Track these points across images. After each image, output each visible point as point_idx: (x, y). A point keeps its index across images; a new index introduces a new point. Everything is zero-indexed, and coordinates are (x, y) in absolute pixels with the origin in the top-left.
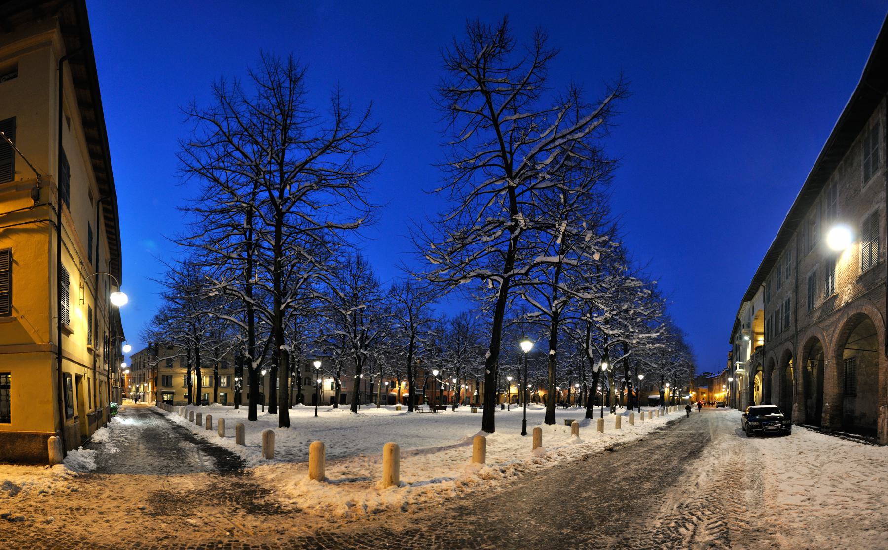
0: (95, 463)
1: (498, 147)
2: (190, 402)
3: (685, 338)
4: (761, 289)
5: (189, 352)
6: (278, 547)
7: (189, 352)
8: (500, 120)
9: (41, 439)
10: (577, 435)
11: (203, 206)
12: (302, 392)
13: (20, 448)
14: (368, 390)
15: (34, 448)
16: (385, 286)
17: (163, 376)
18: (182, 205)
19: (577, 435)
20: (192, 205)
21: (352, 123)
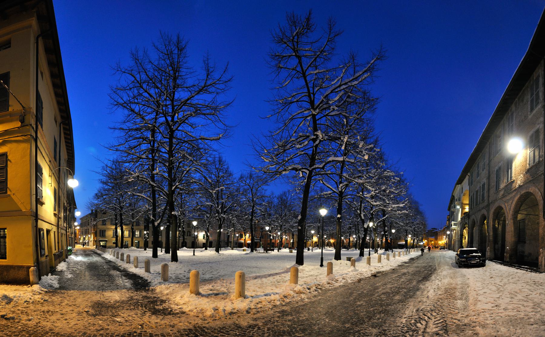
0: (58, 283)
1: (306, 90)
2: (117, 246)
3: (420, 207)
4: (467, 177)
5: (116, 216)
6: (171, 335)
7: (116, 216)
8: (307, 74)
9: (25, 269)
10: (354, 266)
11: (124, 126)
12: (185, 240)
13: (13, 274)
14: (226, 239)
15: (21, 274)
16: (236, 175)
17: (100, 230)
18: (112, 126)
19: (354, 266)
20: (118, 126)
21: (216, 75)
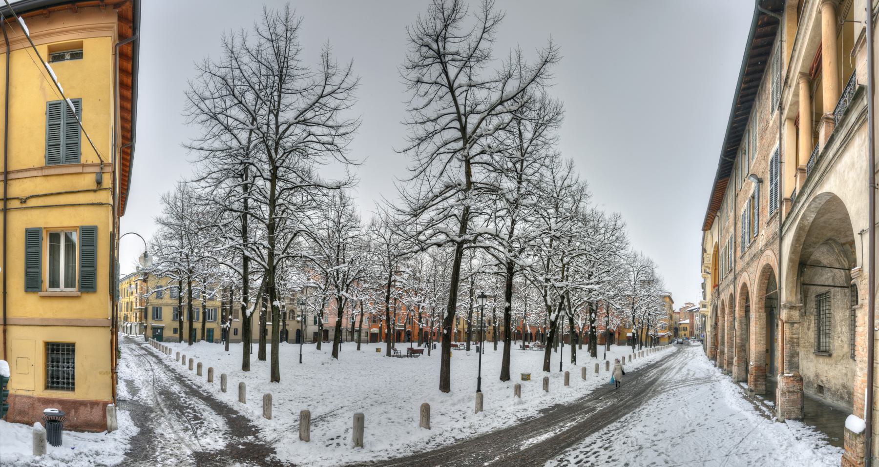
0: (136, 425)
1: (454, 109)
2: (181, 339)
3: (656, 270)
4: (820, 154)
5: (180, 283)
6: (822, 245)
7: (180, 283)
8: (456, 85)
9: (101, 406)
10: (519, 397)
11: (206, 146)
12: (287, 327)
13: (84, 414)
14: (350, 326)
15: (95, 415)
16: (365, 220)
17: (154, 308)
18: (188, 143)
19: (519, 397)
20: (196, 144)
21: (335, 80)
